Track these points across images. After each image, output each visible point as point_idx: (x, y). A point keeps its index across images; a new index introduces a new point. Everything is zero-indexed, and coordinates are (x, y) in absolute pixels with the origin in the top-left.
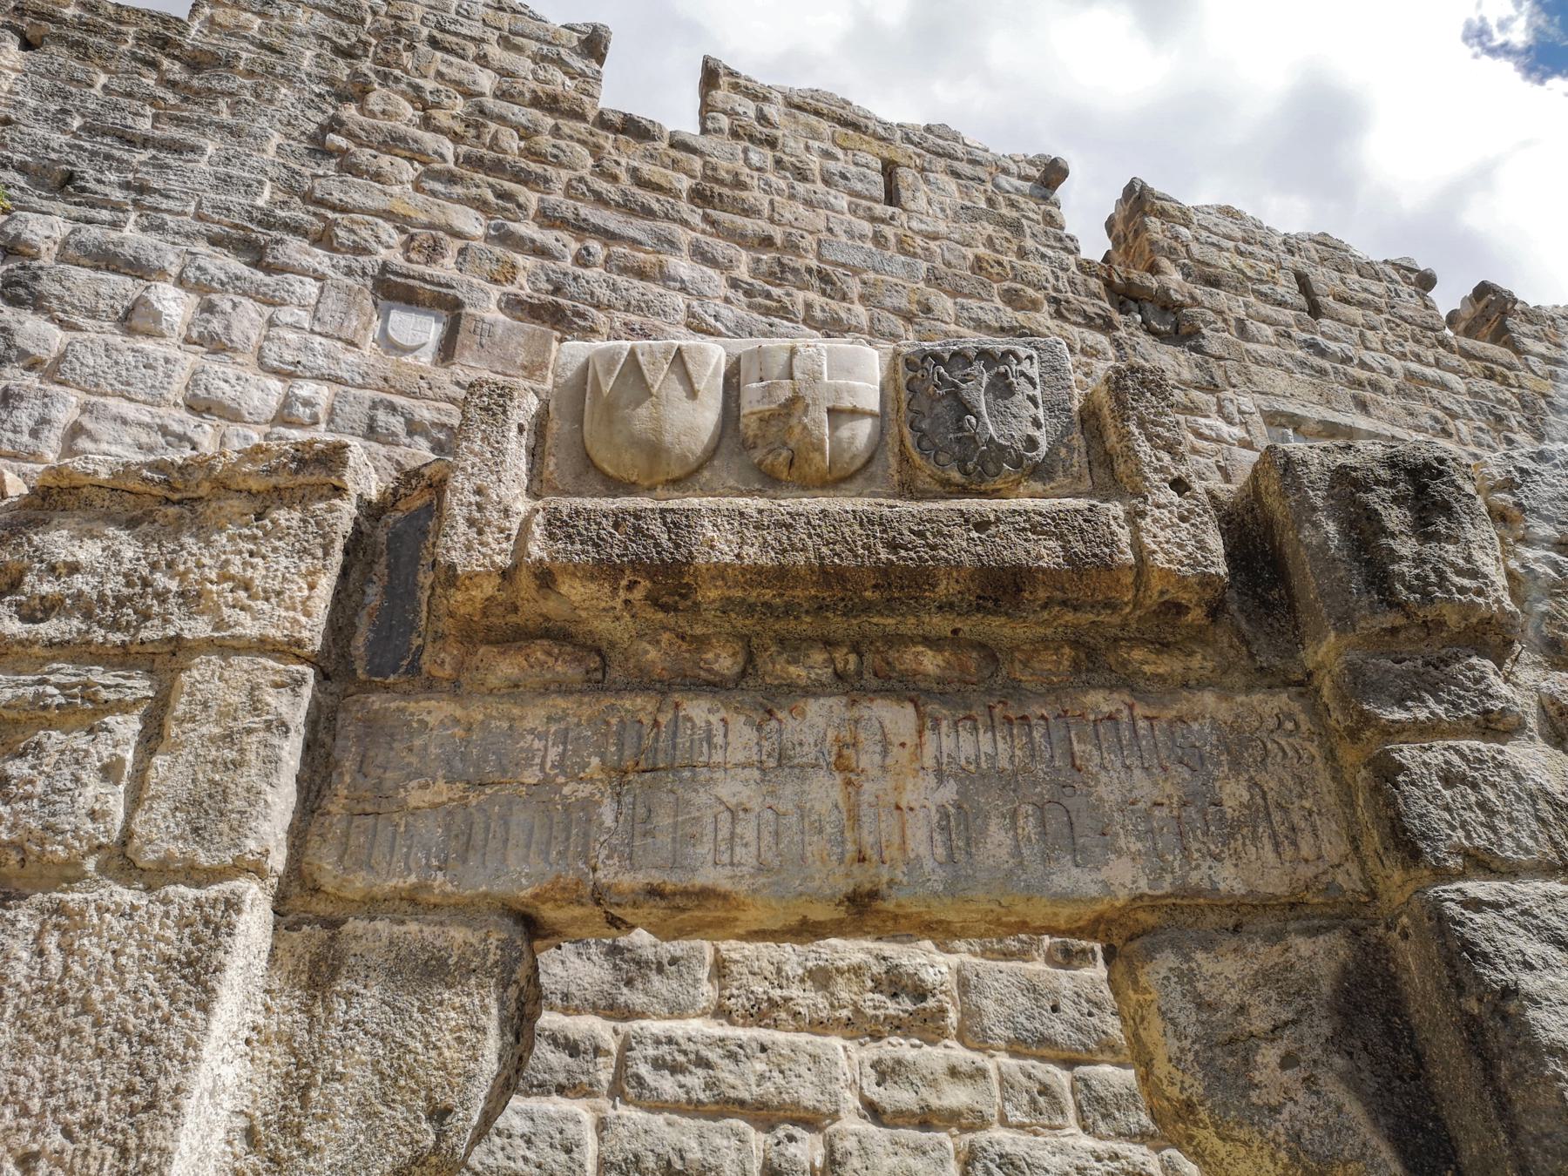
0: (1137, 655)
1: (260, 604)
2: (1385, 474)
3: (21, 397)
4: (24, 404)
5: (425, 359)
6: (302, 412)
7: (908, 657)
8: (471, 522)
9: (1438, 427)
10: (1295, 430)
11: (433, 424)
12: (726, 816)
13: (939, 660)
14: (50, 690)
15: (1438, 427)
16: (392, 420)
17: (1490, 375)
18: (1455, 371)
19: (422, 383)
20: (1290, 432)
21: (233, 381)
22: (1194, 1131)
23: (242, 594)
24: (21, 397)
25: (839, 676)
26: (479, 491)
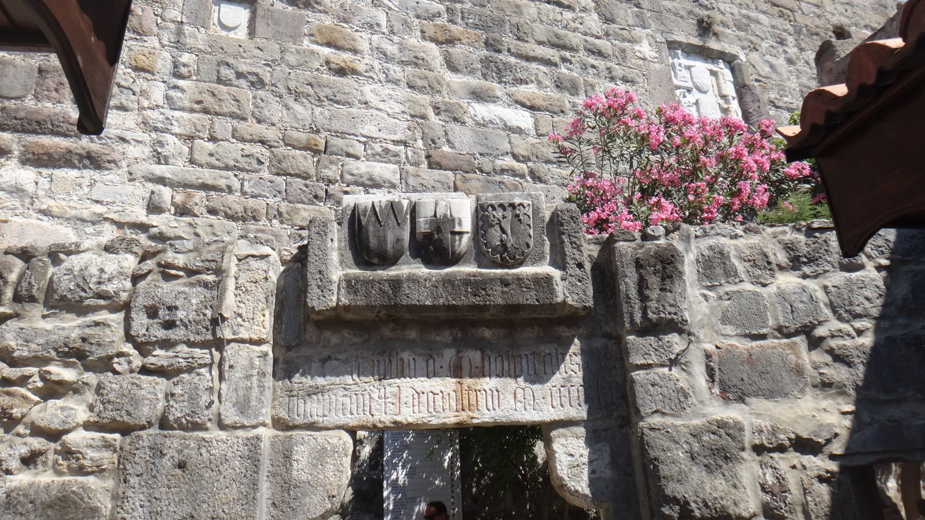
0: (561, 328)
1: (246, 324)
2: (653, 260)
3: (47, 72)
4: (49, 76)
5: (242, 34)
6: (184, 70)
7: (480, 331)
8: (319, 287)
9: (752, 46)
10: (682, 50)
11: (249, 73)
12: (416, 396)
13: (490, 333)
14: (181, 360)
15: (752, 46)
16: (228, 72)
17: (781, 15)
18: (764, 13)
19: (241, 50)
20: (679, 52)
21: (148, 55)
22: (786, 49)
23: (239, 320)
24: (47, 72)
25: (455, 340)
26: (320, 272)
